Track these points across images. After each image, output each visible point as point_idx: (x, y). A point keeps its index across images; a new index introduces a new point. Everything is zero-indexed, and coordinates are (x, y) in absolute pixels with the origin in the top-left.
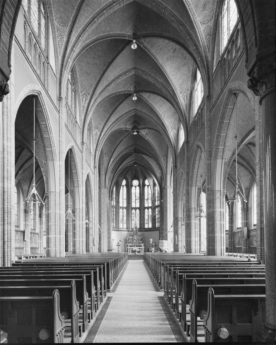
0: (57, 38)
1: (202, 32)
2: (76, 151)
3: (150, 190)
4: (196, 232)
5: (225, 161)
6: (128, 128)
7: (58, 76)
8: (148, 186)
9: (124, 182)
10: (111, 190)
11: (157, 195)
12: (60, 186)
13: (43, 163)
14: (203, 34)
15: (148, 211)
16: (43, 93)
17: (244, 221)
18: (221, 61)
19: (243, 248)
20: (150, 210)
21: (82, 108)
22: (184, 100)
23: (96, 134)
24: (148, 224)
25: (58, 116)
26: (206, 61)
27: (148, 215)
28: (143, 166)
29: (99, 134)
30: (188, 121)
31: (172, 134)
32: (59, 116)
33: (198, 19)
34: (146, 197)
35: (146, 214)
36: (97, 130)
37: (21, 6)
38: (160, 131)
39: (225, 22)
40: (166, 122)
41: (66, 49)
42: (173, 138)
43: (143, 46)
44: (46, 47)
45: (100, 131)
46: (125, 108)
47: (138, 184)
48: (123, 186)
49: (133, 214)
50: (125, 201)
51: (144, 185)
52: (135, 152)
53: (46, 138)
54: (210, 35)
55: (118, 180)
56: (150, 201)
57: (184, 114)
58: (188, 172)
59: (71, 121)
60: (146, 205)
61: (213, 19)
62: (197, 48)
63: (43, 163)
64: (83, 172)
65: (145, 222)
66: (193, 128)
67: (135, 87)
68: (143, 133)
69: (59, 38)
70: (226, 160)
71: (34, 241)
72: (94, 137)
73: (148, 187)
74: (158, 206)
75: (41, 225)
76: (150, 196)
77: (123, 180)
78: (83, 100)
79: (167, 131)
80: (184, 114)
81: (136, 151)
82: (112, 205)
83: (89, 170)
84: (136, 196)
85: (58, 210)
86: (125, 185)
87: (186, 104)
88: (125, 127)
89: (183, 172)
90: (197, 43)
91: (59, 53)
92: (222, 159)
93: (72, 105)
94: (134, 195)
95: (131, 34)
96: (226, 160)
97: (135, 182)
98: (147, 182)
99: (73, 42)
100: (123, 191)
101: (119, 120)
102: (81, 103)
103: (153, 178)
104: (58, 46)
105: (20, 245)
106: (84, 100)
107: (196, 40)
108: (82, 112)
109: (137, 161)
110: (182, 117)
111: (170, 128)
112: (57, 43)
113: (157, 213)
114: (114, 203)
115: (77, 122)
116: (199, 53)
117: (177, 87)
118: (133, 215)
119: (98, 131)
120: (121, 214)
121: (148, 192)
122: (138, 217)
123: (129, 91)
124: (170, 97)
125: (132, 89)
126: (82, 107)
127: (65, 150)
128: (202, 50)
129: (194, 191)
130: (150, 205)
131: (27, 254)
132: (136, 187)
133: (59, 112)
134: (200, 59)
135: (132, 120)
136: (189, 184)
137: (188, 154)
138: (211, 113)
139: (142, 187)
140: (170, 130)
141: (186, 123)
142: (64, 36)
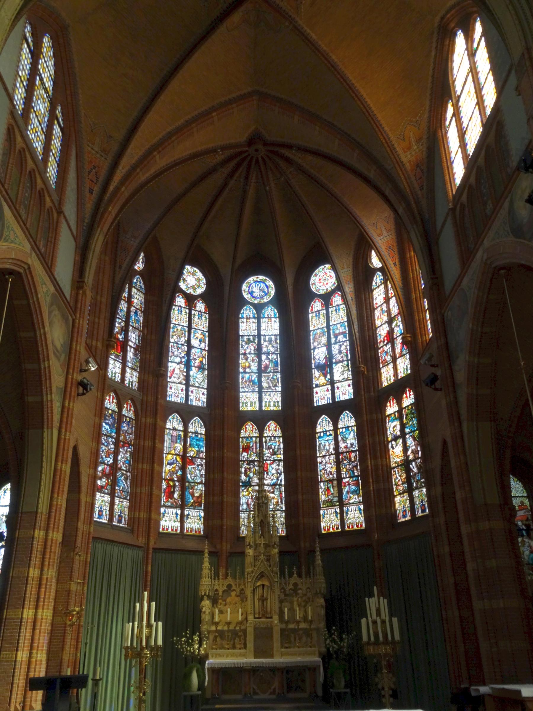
8: (326, 298)
15: (336, 429)
20: (347, 420)
24: (342, 504)
34: (319, 354)
35: (325, 445)
48: (190, 300)
49: (246, 449)
50: (199, 378)
51: (305, 296)
56: (341, 372)
60: (321, 396)
65: (323, 497)
76: (342, 348)
86: (202, 296)
94: (252, 347)
97: (258, 288)
100: (189, 327)
113: (393, 427)
118: (244, 455)
120: (171, 450)
122: (275, 473)
132: (259, 308)
139: (293, 305)
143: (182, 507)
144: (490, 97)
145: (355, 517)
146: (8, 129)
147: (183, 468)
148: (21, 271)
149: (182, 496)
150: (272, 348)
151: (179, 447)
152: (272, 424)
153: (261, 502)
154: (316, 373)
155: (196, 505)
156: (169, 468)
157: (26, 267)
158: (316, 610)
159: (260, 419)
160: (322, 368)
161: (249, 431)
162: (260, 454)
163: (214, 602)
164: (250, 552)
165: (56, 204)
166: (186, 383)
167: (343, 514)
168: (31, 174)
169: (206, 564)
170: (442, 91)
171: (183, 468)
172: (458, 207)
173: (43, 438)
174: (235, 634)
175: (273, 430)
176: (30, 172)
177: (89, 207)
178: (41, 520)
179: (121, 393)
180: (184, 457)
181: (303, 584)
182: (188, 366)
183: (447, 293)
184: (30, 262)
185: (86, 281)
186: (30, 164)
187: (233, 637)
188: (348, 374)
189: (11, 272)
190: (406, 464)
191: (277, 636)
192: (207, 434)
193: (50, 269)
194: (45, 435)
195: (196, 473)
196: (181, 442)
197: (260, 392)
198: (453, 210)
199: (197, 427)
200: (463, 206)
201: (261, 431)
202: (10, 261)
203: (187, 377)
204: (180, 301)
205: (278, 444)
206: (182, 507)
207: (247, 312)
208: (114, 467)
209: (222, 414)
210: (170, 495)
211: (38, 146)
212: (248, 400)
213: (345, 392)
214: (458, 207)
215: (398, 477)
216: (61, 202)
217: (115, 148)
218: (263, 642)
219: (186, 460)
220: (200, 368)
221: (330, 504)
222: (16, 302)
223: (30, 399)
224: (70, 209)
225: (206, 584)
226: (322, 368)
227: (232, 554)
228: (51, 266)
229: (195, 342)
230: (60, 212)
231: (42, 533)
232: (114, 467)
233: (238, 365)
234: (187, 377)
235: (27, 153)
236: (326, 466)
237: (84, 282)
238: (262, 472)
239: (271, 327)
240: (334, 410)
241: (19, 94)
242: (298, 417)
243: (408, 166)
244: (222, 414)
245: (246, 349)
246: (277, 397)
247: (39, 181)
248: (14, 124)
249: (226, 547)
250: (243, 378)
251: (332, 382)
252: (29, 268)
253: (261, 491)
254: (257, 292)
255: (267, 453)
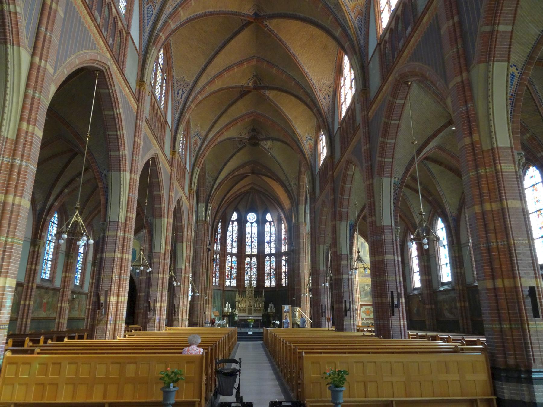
0: (145, 5)
1: (350, 10)
3: (273, 229)
4: (398, 282)
7: (142, 53)
8: (270, 223)
9: (235, 216)
10: (214, 226)
11: (283, 236)
14: (351, 12)
16: (114, 69)
17: (424, 278)
19: (427, 322)
20: (273, 258)
21: (176, 103)
23: (196, 143)
24: (270, 280)
25: (136, 106)
27: (270, 267)
29: (199, 143)
30: (331, 128)
31: (307, 146)
32: (138, 107)
34: (267, 239)
35: (267, 264)
36: (197, 137)
38: (291, 142)
41: (157, 20)
44: (126, 12)
46: (240, 108)
47: (256, 218)
48: (233, 222)
49: (247, 264)
50: (235, 245)
51: (265, 221)
52: (253, 173)
54: (361, 14)
56: (273, 245)
60: (267, 251)
63: (103, 175)
64: (171, 194)
65: (266, 278)
66: (343, 135)
67: (255, 82)
69: (148, 5)
70: (396, 179)
71: (77, 306)
72: (192, 147)
73: (270, 224)
74: (285, 254)
75: (38, 252)
76: (273, 238)
77: (233, 213)
78: (178, 94)
82: (215, 249)
84: (251, 238)
85: (161, 288)
86: (236, 220)
90: (344, 24)
91: (146, 24)
93: (161, 97)
94: (250, 235)
95: (252, 14)
96: (396, 179)
97: (252, 217)
98: (269, 217)
99: (168, 13)
100: (233, 230)
102: (176, 97)
104: (146, 15)
105: (49, 313)
106: (180, 93)
107: (342, 21)
111: (304, 138)
112: (146, 12)
113: (284, 263)
114: (219, 247)
118: (246, 266)
119: (199, 139)
120: (228, 265)
121: (270, 230)
122: (254, 270)
123: (246, 87)
124: (305, 96)
125: (250, 85)
127: (143, 157)
128: (351, 32)
129: (344, 228)
130: (273, 251)
131: (59, 330)
132: (252, 223)
134: (348, 43)
136: (336, 216)
139: (261, 222)
142: (156, 4)
143: (231, 279)
145: (273, 284)
147: (231, 270)
148: (104, 69)
149: (231, 277)
150: (255, 235)
151: (230, 264)
152: (254, 258)
153: (250, 281)
154: (266, 244)
155: (234, 279)
156: (228, 270)
158: (262, 305)
159: (251, 256)
160: (268, 243)
161: (248, 259)
162: (251, 266)
163: (239, 302)
164: (247, 292)
165: (126, 27)
166: (232, 247)
167: (270, 283)
169: (237, 294)
171: (231, 270)
172: (383, 43)
173: (6, 54)
174: (243, 310)
175: (254, 259)
177: (177, 116)
178: (183, 271)
179: (216, 252)
180: (231, 267)
181: (259, 299)
182: (232, 241)
185: (145, 80)
187: (243, 310)
188: (274, 246)
189: (98, 70)
190: (285, 272)
191: (253, 311)
192: (237, 260)
193: (163, 149)
194: (10, 51)
195: (234, 271)
196: (231, 262)
197: (251, 249)
199: (234, 258)
201: (251, 259)
202: (97, 62)
203: (232, 245)
204: (231, 223)
205: (256, 263)
206: (231, 279)
207: (248, 224)
208: (216, 271)
209: (241, 255)
210: (228, 277)
212: (248, 251)
213: (273, 251)
214: (383, 43)
215: (283, 275)
216: (129, 27)
217: (219, 203)
218: (250, 311)
219: (232, 268)
220: (235, 242)
221: (268, 279)
222: (102, 91)
223: (112, 153)
224: (135, 32)
225: (237, 298)
226: (268, 243)
227: (243, 291)
228: (123, 67)
229: (234, 235)
230: (128, 33)
231: (163, 261)
232: (216, 271)
233: (245, 240)
234: (232, 245)
235: (112, 6)
236: (267, 270)
238: (251, 270)
239: (255, 229)
240: (270, 255)
242: (261, 256)
244: (241, 255)
245: (248, 236)
246: (256, 250)
249: (241, 289)
250: (247, 244)
251: (270, 247)
252: (109, 68)
253: (251, 276)
254: (251, 219)
255: (252, 265)
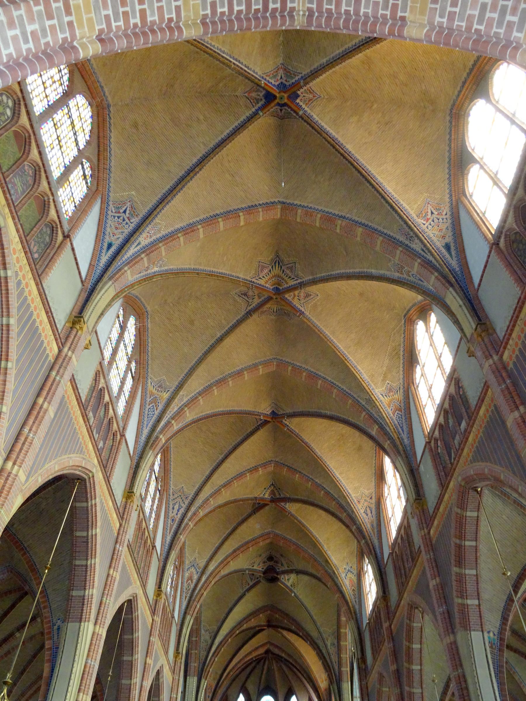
2: (143, 611)
5: (489, 637)
6: (255, 570)
12: (79, 692)
13: (56, 627)
16: (99, 477)
18: (430, 442)
21: (170, 521)
22: (367, 515)
23: (190, 578)
25: (118, 525)
26: (401, 444)
28: (285, 660)
29: (195, 577)
30: (378, 551)
31: (346, 581)
33: (376, 391)
36: (193, 570)
37: (84, 275)
38: (323, 576)
39: (422, 392)
40: (333, 558)
42: (351, 592)
43: (288, 429)
44: (125, 413)
45: (200, 571)
46: (254, 527)
53: (79, 566)
55: (227, 696)
57: (370, 539)
58: (398, 670)
59: (143, 542)
61: (401, 391)
62: (382, 428)
64: (149, 661)
68: (286, 583)
72: (185, 585)
77: (238, 696)
79: (337, 578)
80: (370, 539)
81: (270, 625)
83: (163, 661)
87: (372, 522)
88: (251, 567)
89: (385, 674)
92: (482, 631)
95: (269, 413)
96: (491, 634)
99: (172, 413)
101: (246, 473)
103: (308, 692)
108: (169, 528)
109: (271, 648)
110: (366, 543)
112: (146, 412)
115: (155, 546)
116: (386, 434)
117: (350, 491)
119: (195, 573)
124: (340, 512)
126: (169, 520)
133: (122, 518)
135: (264, 556)
137: (390, 626)
138: (430, 531)
140: (343, 575)
141: (376, 554)
144: (448, 361)
146: (96, 374)
157: (91, 475)
165: (121, 429)
168: (106, 406)
170: (411, 359)
176: (105, 405)
183: (431, 512)
184: (94, 471)
186: (107, 398)
193: (144, 586)
198: (369, 623)
200: (436, 440)
211: (115, 389)
228: (42, 273)
230: (123, 436)
237: (133, 492)
241: (107, 354)
243: (323, 690)
247: (111, 411)
248: (100, 370)
